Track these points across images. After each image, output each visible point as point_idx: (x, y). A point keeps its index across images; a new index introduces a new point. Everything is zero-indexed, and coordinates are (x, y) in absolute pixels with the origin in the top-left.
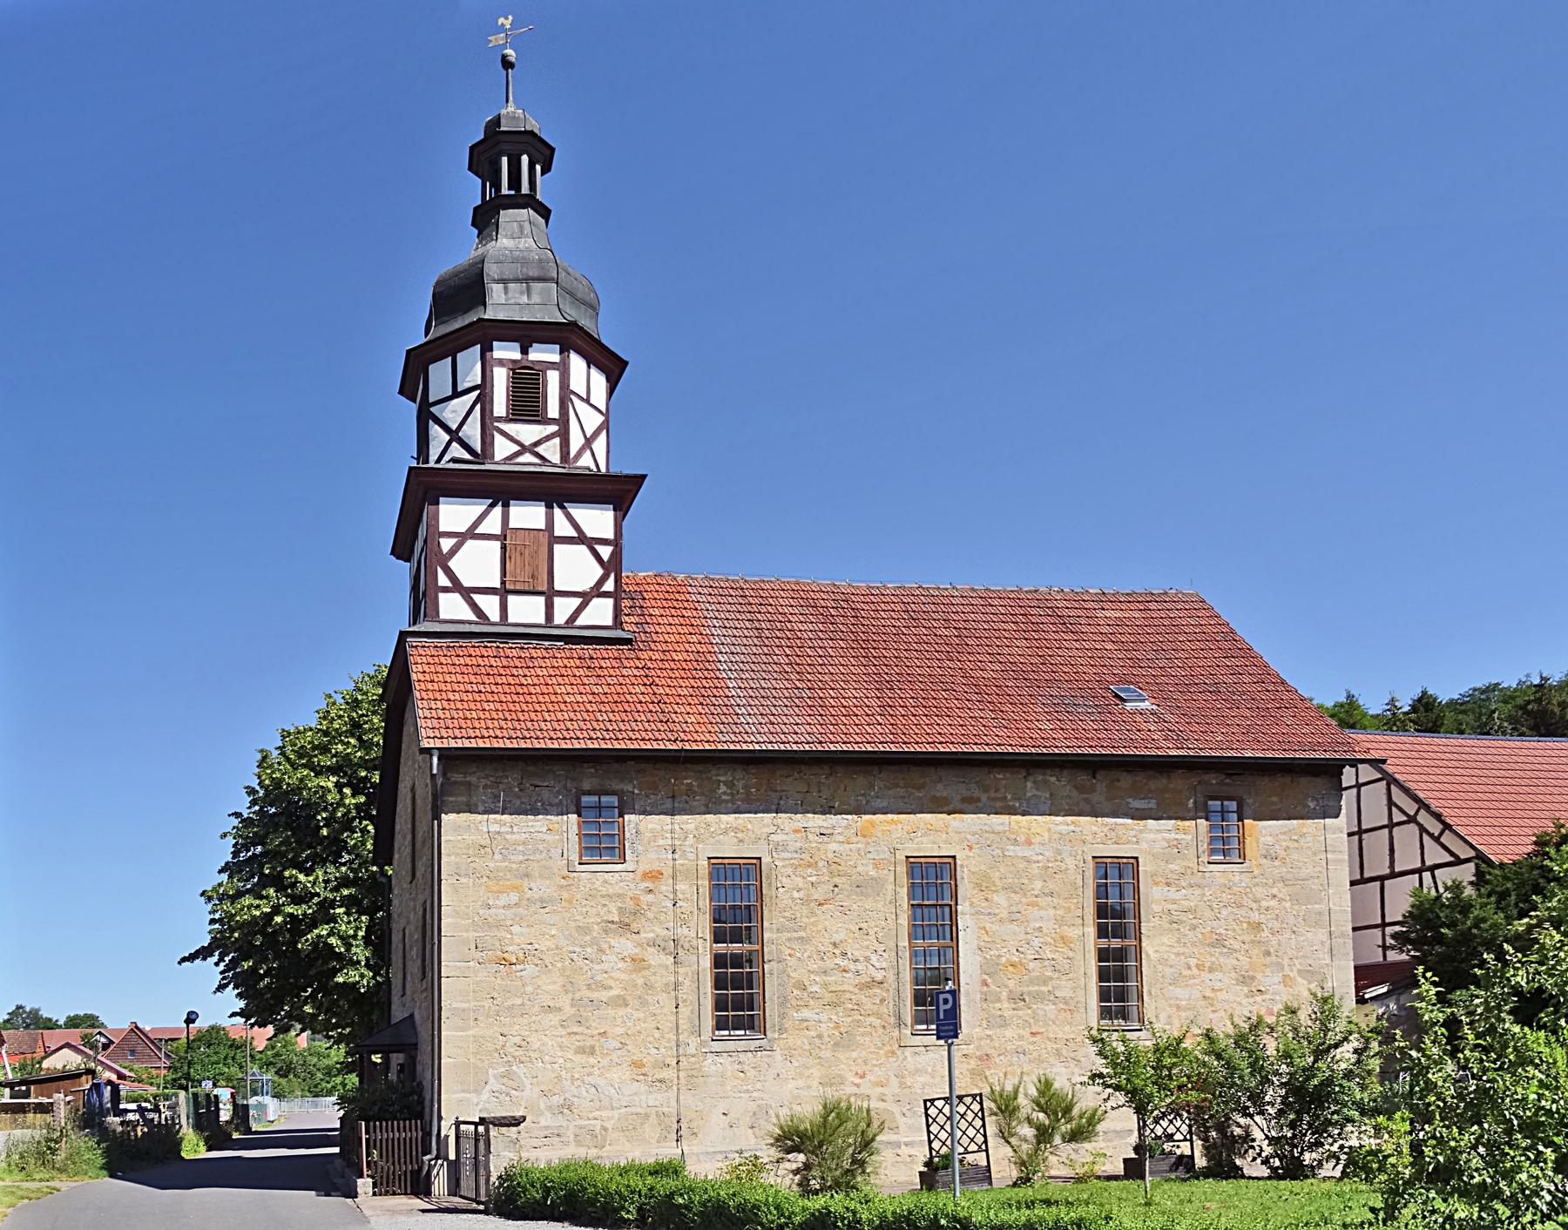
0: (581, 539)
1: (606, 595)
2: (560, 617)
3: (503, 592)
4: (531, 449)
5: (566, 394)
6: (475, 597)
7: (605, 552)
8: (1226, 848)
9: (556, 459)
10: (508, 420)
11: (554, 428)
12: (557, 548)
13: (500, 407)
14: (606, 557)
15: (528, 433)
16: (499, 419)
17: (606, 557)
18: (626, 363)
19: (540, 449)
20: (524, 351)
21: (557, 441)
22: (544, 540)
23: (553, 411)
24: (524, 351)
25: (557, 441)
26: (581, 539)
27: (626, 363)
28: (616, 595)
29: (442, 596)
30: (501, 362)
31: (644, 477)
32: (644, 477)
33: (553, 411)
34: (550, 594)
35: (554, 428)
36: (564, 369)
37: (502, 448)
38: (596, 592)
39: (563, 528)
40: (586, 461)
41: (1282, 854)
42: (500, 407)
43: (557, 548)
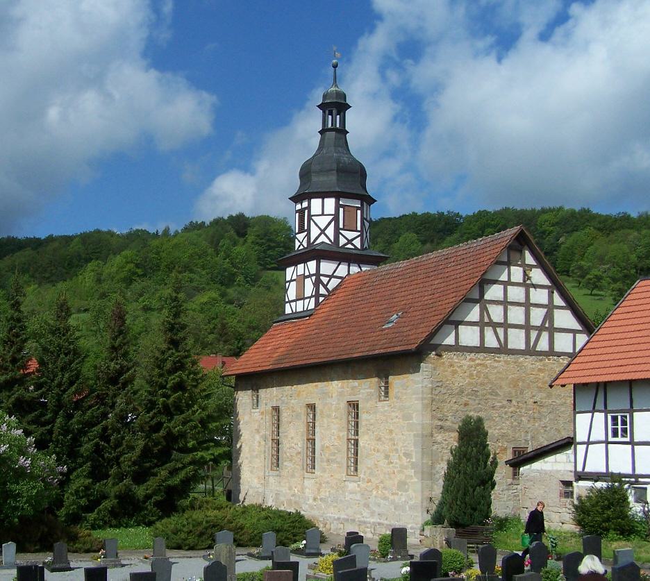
4: (350, 242)
15: (350, 235)
21: (359, 238)
25: (359, 238)
36: (309, 208)
37: (342, 241)
40: (323, 239)
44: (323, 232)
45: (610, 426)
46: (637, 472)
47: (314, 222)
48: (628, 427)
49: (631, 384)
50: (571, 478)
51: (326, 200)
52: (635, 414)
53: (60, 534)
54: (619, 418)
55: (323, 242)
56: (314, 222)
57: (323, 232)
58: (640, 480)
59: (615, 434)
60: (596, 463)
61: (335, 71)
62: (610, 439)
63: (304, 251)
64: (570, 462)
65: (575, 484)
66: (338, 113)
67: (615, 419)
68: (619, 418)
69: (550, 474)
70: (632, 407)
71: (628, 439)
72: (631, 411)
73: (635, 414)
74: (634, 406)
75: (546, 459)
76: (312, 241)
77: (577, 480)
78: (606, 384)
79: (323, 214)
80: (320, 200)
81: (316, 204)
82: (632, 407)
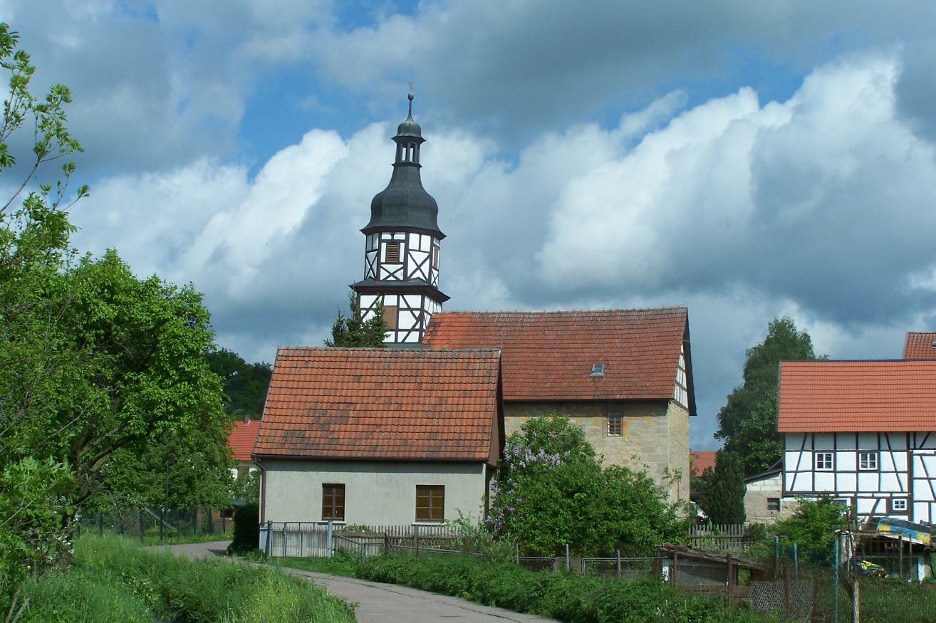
0: (409, 309)
1: (417, 330)
2: (400, 340)
3: (398, 309)
4: (392, 274)
5: (407, 251)
6: (429, 260)
7: (417, 313)
8: (616, 429)
9: (401, 278)
10: (386, 263)
11: (402, 266)
12: (400, 312)
13: (383, 259)
14: (417, 316)
15: (392, 268)
16: (383, 263)
17: (417, 316)
18: (344, 485)
19: (396, 274)
20: (393, 236)
21: (402, 271)
22: (396, 309)
23: (402, 259)
24: (393, 236)
25: (402, 271)
26: (409, 309)
27: (344, 485)
28: (421, 330)
29: (396, 296)
30: (384, 241)
31: (361, 230)
32: (361, 230)
33: (402, 259)
34: (397, 330)
35: (402, 266)
36: (407, 241)
37: (383, 275)
38: (413, 329)
39: (402, 305)
40: (418, 274)
41: (639, 433)
42: (383, 259)
43: (400, 312)
44: (419, 267)
45: (876, 461)
46: (838, 490)
47: (411, 256)
48: (832, 461)
49: (835, 435)
50: (778, 495)
51: (423, 236)
52: (837, 453)
53: (221, 618)
54: (824, 456)
55: (419, 278)
56: (411, 256)
57: (419, 267)
58: (840, 495)
59: (820, 465)
60: (803, 483)
61: (410, 103)
62: (861, 468)
63: (393, 284)
64: (778, 485)
65: (781, 500)
66: (413, 146)
67: (820, 457)
68: (824, 456)
69: (759, 494)
70: (835, 448)
71: (832, 469)
72: (835, 451)
73: (837, 453)
74: (815, 447)
75: (754, 483)
76: (408, 275)
77: (783, 497)
78: (813, 435)
79: (419, 250)
80: (417, 236)
81: (414, 237)
82: (835, 448)
